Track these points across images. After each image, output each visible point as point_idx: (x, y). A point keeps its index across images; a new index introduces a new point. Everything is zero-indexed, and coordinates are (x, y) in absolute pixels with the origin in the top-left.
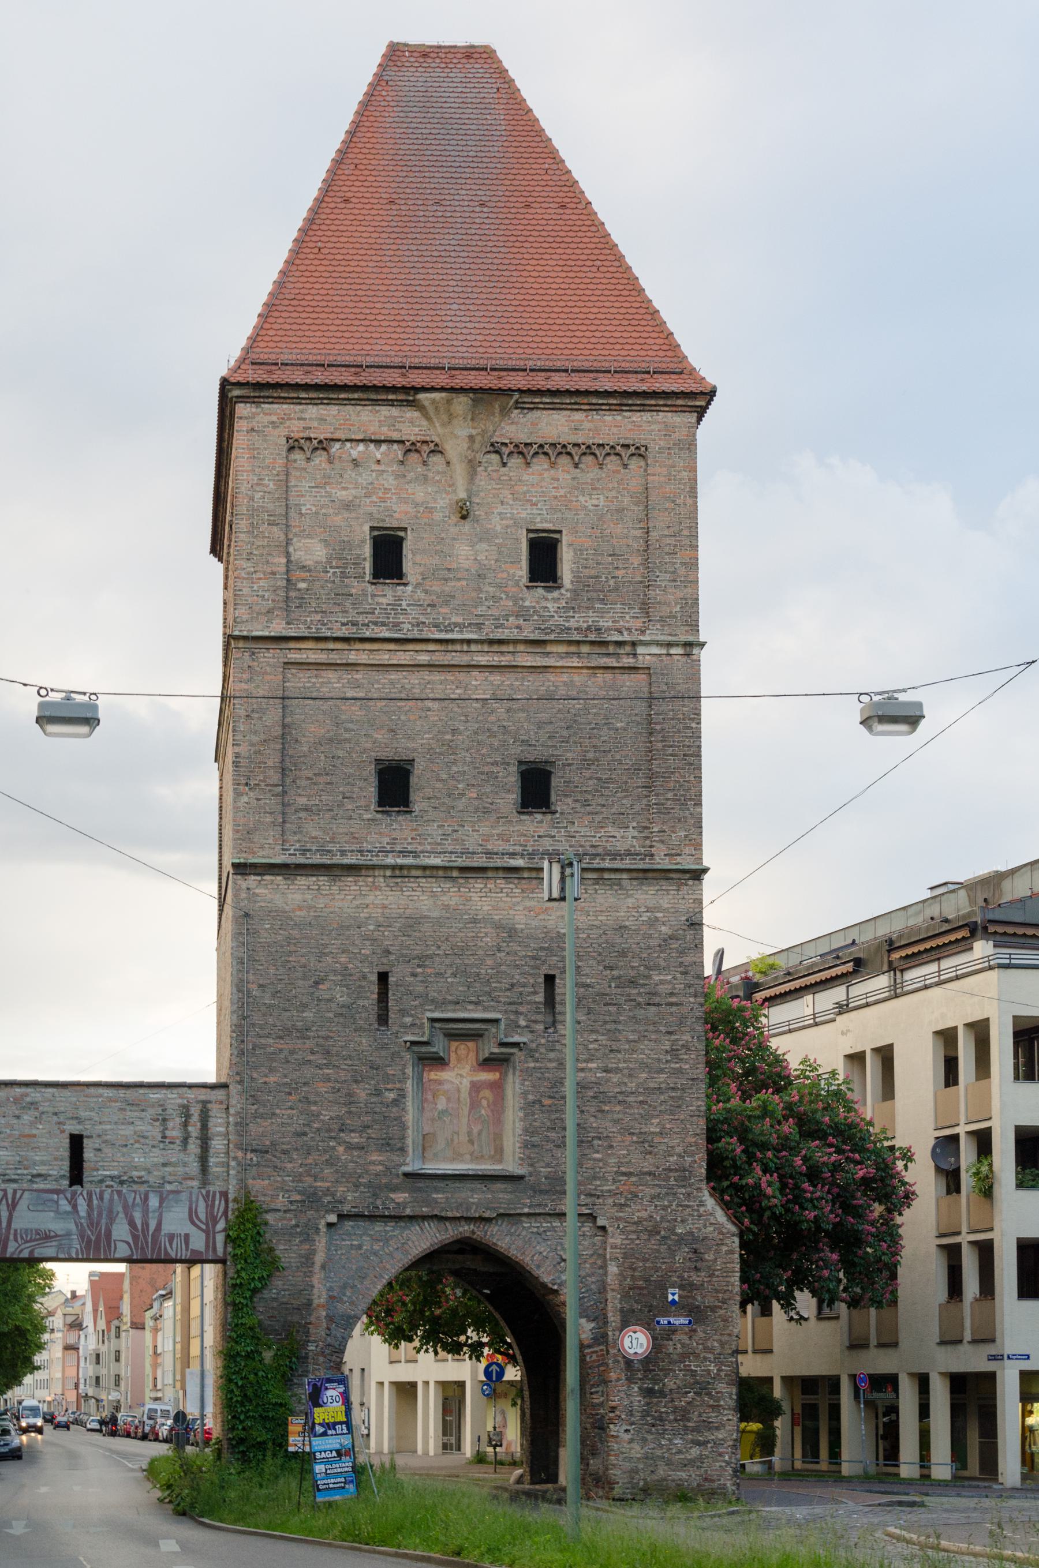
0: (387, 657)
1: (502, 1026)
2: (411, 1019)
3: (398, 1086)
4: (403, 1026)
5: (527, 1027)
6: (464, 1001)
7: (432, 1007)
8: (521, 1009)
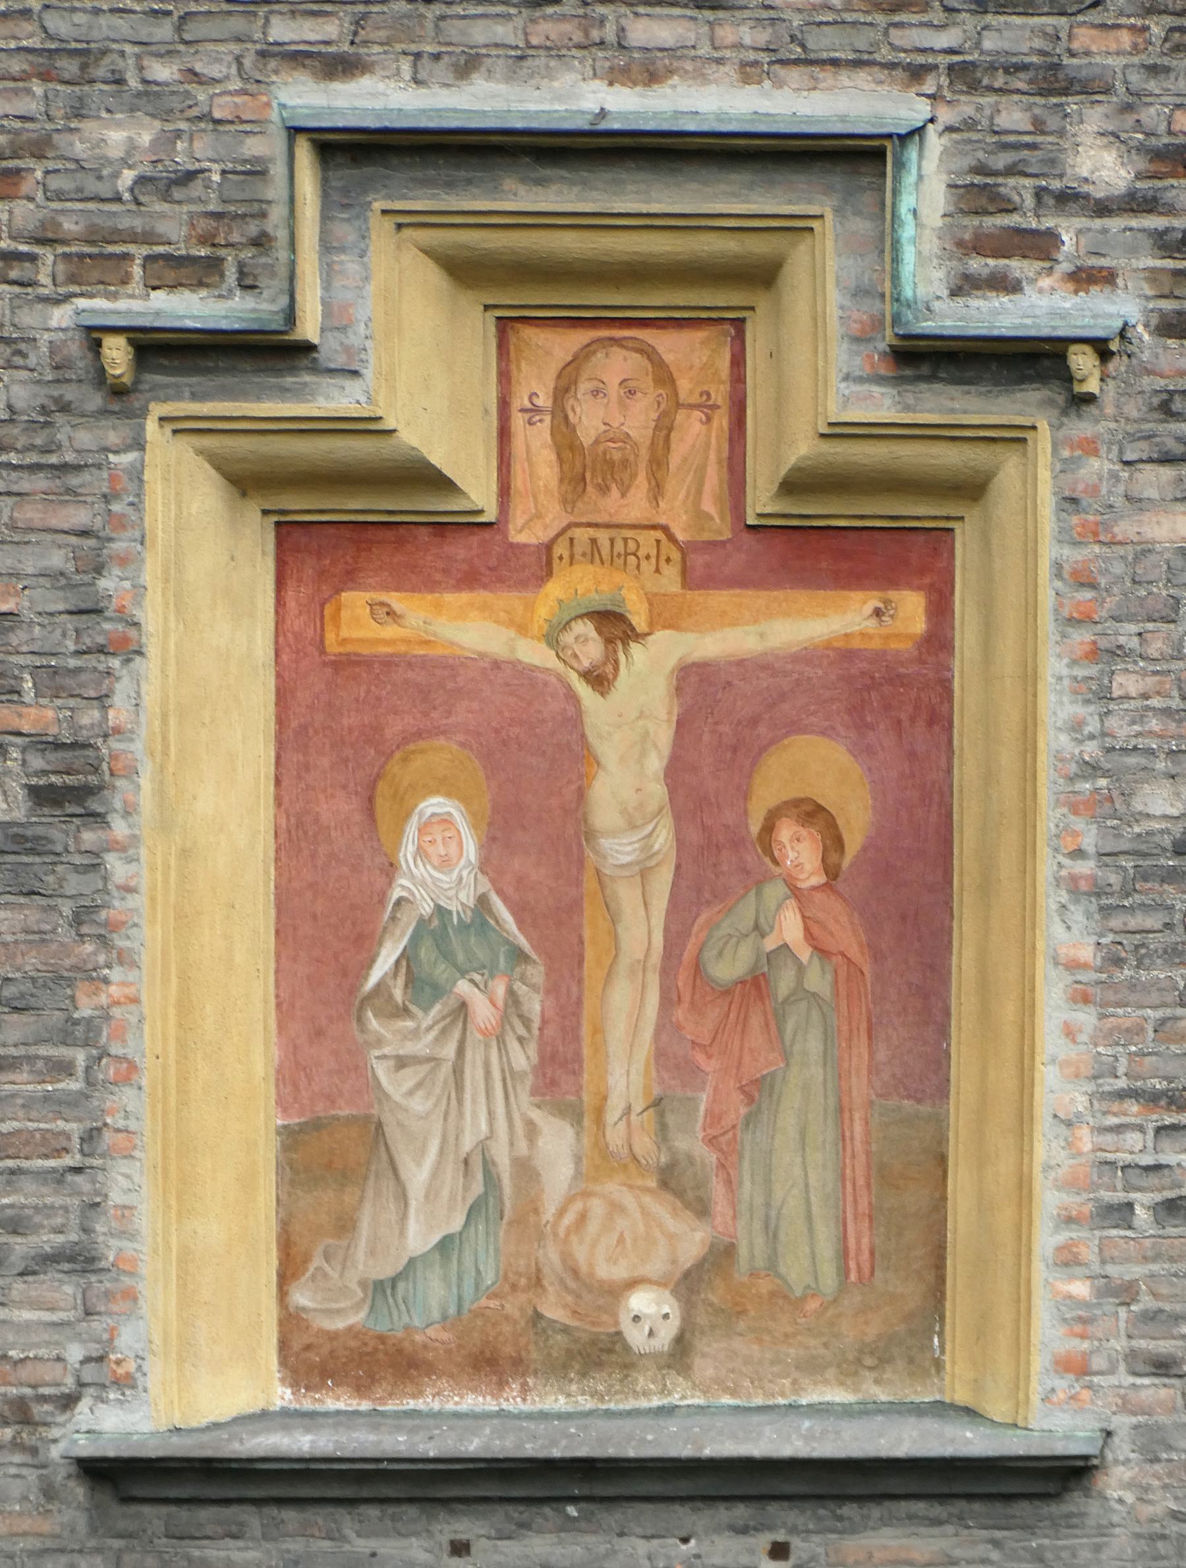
5: (1134, 203)
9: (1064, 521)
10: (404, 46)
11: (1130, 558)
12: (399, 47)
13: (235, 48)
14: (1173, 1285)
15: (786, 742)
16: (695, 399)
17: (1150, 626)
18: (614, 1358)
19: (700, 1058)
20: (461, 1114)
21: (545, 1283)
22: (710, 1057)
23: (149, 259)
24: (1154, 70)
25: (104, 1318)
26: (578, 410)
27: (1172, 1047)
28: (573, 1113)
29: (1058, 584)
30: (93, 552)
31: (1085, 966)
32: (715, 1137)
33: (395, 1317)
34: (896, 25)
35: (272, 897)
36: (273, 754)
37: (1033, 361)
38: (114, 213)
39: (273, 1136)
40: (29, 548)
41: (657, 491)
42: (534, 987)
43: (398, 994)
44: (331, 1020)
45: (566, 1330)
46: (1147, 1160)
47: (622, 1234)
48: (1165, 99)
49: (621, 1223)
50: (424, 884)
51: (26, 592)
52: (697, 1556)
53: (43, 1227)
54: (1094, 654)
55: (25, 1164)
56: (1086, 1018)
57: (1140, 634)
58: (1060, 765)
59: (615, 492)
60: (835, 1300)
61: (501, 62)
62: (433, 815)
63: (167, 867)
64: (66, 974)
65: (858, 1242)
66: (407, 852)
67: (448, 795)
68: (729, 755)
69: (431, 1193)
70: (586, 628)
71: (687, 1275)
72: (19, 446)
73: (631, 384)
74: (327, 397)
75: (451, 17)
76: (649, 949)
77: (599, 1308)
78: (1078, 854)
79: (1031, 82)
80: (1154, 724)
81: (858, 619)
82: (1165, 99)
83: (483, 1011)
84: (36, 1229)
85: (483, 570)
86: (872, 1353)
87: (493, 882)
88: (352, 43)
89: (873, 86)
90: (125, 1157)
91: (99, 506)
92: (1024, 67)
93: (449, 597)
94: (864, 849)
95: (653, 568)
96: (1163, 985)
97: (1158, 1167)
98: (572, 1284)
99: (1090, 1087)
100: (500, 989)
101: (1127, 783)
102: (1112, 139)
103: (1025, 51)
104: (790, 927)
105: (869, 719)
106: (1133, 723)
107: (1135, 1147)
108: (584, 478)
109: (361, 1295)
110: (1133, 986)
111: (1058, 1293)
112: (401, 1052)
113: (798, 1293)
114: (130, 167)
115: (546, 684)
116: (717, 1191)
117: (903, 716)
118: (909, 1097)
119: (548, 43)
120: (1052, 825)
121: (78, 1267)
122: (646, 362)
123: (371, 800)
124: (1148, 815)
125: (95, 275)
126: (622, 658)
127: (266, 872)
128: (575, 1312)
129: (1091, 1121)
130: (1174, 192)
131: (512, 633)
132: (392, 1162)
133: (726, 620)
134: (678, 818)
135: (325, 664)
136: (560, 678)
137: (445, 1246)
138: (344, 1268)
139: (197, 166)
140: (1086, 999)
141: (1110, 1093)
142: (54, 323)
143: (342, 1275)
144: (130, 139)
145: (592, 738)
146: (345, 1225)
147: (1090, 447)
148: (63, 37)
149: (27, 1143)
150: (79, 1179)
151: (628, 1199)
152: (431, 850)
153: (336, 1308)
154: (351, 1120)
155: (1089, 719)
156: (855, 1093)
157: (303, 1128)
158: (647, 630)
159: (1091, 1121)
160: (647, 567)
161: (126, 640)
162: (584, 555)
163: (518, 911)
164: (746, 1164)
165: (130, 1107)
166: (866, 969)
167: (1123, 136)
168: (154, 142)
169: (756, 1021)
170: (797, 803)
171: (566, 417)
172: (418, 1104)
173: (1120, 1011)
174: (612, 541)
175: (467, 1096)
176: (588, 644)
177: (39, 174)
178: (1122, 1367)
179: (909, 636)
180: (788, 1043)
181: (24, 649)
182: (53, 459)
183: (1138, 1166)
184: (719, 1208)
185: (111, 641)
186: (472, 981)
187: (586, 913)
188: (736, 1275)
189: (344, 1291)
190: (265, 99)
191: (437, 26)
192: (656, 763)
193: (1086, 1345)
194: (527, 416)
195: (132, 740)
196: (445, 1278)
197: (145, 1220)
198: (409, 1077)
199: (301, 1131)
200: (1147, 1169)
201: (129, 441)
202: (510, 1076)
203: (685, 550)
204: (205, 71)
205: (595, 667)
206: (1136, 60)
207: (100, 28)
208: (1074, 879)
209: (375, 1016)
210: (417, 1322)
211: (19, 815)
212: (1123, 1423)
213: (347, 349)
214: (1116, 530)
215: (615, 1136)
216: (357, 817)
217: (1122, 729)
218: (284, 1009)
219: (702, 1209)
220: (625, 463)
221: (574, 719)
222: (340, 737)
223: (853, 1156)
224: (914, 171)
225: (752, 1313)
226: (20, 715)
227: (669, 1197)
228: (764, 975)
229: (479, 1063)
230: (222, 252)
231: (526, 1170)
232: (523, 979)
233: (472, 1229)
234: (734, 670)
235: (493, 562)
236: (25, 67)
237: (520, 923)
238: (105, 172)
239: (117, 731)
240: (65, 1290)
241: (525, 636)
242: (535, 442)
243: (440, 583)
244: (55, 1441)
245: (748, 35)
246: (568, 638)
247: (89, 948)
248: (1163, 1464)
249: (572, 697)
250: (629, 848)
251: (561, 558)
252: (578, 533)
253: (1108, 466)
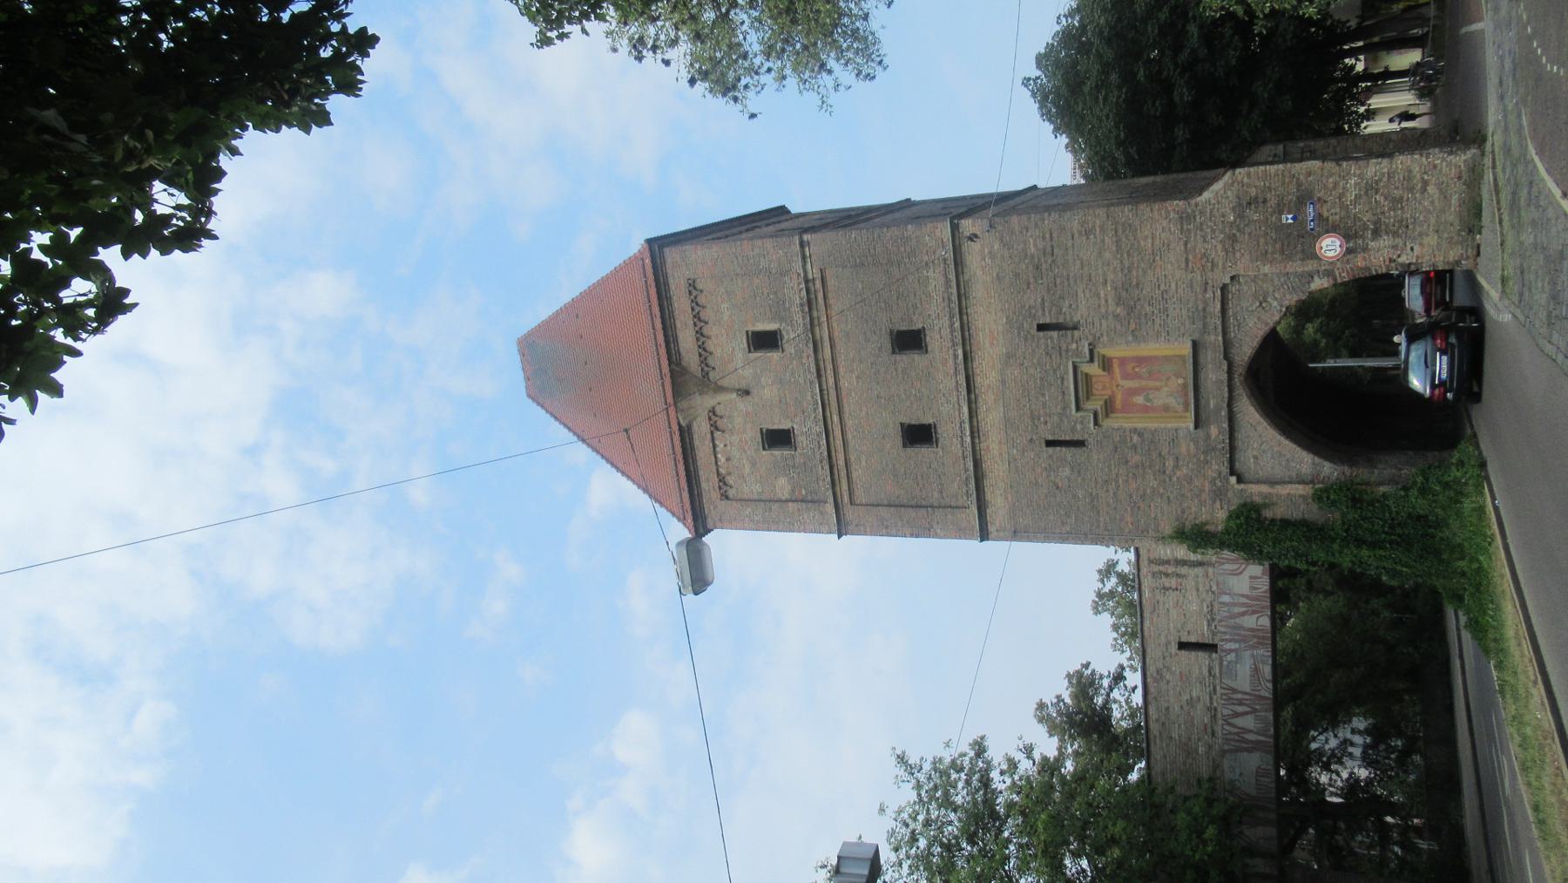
37: (1091, 351)
153: (1180, 408)
222: (1128, 408)
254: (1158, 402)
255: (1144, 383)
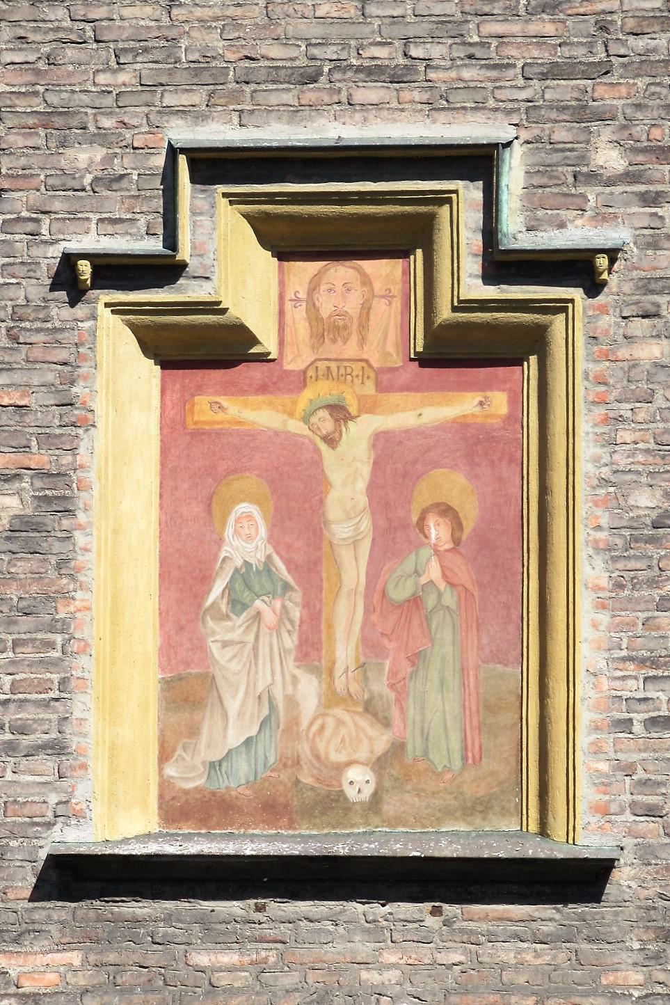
0: (641, 826)
1: (514, 174)
2: (99, 153)
3: (40, 458)
4: (68, 184)
5: (630, 177)
6: (339, 65)
7: (198, 97)
8: (609, 95)
9: (590, 349)
10: (234, 107)
11: (626, 369)
12: (231, 107)
13: (146, 109)
14: (654, 764)
15: (431, 473)
16: (383, 293)
17: (638, 405)
18: (339, 804)
19: (386, 641)
20: (257, 672)
21: (302, 763)
22: (390, 641)
23: (101, 220)
24: (638, 106)
25: (69, 780)
26: (320, 300)
27: (653, 633)
28: (315, 670)
29: (586, 383)
30: (70, 370)
31: (603, 589)
32: (394, 684)
33: (221, 781)
34: (497, 88)
35: (158, 557)
36: (159, 481)
38: (81, 197)
39: (156, 682)
40: (36, 372)
41: (363, 341)
42: (296, 604)
43: (224, 607)
44: (188, 621)
45: (313, 789)
46: (640, 695)
47: (343, 737)
48: (645, 122)
49: (343, 731)
50: (237, 549)
51: (34, 395)
52: (391, 914)
53: (37, 730)
54: (606, 420)
55: (29, 696)
56: (604, 618)
57: (632, 409)
58: (588, 480)
59: (340, 342)
60: (460, 774)
61: (285, 113)
62: (243, 513)
63: (107, 539)
64: (52, 595)
65: (473, 742)
66: (229, 532)
67: (250, 502)
68: (401, 480)
69: (241, 714)
70: (324, 414)
71: (379, 759)
72: (31, 319)
73: (349, 285)
74: (194, 291)
75: (260, 91)
76: (358, 584)
77: (331, 777)
78: (599, 528)
79: (572, 115)
80: (640, 458)
81: (470, 408)
82: (645, 122)
83: (269, 617)
84: (34, 731)
85: (270, 384)
86: (481, 804)
87: (275, 548)
88: (207, 105)
89: (485, 121)
90: (82, 692)
91: (73, 350)
92: (565, 108)
93: (251, 398)
94: (474, 530)
95: (361, 381)
96: (647, 598)
97: (645, 700)
98: (317, 765)
99: (606, 655)
100: (278, 604)
101: (626, 489)
102: (616, 144)
103: (568, 99)
104: (434, 572)
105: (476, 460)
106: (628, 457)
107: (633, 688)
108: (323, 335)
109: (203, 769)
110: (630, 600)
111: (590, 768)
112: (225, 639)
113: (440, 770)
114: (90, 173)
115: (303, 443)
116: (395, 713)
117: (495, 458)
118: (499, 663)
119: (311, 103)
120: (584, 513)
121: (55, 752)
122: (357, 273)
123: (210, 505)
124: (638, 507)
125: (72, 229)
126: (344, 429)
127: (155, 543)
128: (318, 779)
129: (608, 674)
130: (650, 171)
131: (285, 417)
132: (220, 697)
133: (396, 409)
134: (373, 513)
135: (186, 434)
136: (311, 441)
137: (248, 742)
138: (193, 755)
139: (125, 172)
140: (604, 607)
141: (618, 658)
142: (49, 255)
143: (192, 758)
144: (90, 158)
145: (327, 471)
146: (194, 731)
147: (603, 310)
148: (56, 105)
149: (30, 685)
150: (57, 704)
151: (347, 718)
152: (241, 531)
153: (189, 775)
154: (199, 676)
155: (604, 455)
156: (470, 660)
157: (172, 680)
158: (357, 414)
159: (608, 674)
160: (357, 382)
161: (86, 419)
162: (323, 375)
163: (288, 563)
164: (411, 700)
165: (83, 665)
166: (476, 594)
167: (622, 143)
168: (103, 159)
169: (415, 622)
170: (437, 505)
171: (314, 304)
172: (234, 666)
173: (623, 613)
174: (338, 368)
175: (260, 662)
176: (325, 422)
177: (42, 177)
178: (628, 811)
179: (498, 416)
180: (433, 634)
181: (33, 424)
182: (49, 325)
183: (634, 698)
184: (396, 723)
185: (78, 420)
186: (263, 600)
187: (324, 564)
188: (406, 760)
189: (193, 768)
190: (161, 136)
191: (252, 96)
192: (362, 485)
193: (607, 797)
194: (293, 303)
195: (89, 471)
196: (248, 760)
197: (91, 727)
198: (230, 652)
199: (172, 681)
200: (640, 700)
201: (89, 315)
202: (283, 652)
203: (378, 372)
204: (130, 122)
205: (328, 434)
206: (629, 101)
207: (75, 100)
208: (596, 541)
209: (212, 619)
210: (232, 785)
211: (29, 511)
212: (629, 842)
213: (205, 267)
214: (618, 354)
215: (340, 684)
216: (203, 514)
217: (622, 461)
218: (163, 615)
219: (387, 724)
220: (345, 327)
221: (317, 462)
222: (195, 470)
223: (470, 695)
224: (508, 164)
225: (415, 780)
226: (30, 459)
227: (369, 716)
228: (420, 597)
229: (267, 643)
230: (138, 216)
231: (292, 702)
232: (290, 600)
233: (263, 734)
234: (403, 435)
235: (275, 379)
236: (36, 121)
237: (289, 570)
238: (77, 176)
239: (81, 467)
240: (47, 764)
241: (292, 418)
242: (298, 317)
243: (247, 391)
244: (41, 847)
245: (417, 96)
246: (314, 419)
247: (65, 581)
248: (653, 866)
249: (317, 451)
250: (347, 530)
251: (311, 377)
252: (319, 364)
253: (613, 319)
254: (225, 642)
255: (353, 570)
